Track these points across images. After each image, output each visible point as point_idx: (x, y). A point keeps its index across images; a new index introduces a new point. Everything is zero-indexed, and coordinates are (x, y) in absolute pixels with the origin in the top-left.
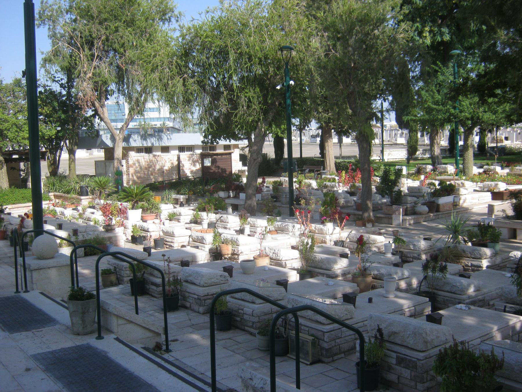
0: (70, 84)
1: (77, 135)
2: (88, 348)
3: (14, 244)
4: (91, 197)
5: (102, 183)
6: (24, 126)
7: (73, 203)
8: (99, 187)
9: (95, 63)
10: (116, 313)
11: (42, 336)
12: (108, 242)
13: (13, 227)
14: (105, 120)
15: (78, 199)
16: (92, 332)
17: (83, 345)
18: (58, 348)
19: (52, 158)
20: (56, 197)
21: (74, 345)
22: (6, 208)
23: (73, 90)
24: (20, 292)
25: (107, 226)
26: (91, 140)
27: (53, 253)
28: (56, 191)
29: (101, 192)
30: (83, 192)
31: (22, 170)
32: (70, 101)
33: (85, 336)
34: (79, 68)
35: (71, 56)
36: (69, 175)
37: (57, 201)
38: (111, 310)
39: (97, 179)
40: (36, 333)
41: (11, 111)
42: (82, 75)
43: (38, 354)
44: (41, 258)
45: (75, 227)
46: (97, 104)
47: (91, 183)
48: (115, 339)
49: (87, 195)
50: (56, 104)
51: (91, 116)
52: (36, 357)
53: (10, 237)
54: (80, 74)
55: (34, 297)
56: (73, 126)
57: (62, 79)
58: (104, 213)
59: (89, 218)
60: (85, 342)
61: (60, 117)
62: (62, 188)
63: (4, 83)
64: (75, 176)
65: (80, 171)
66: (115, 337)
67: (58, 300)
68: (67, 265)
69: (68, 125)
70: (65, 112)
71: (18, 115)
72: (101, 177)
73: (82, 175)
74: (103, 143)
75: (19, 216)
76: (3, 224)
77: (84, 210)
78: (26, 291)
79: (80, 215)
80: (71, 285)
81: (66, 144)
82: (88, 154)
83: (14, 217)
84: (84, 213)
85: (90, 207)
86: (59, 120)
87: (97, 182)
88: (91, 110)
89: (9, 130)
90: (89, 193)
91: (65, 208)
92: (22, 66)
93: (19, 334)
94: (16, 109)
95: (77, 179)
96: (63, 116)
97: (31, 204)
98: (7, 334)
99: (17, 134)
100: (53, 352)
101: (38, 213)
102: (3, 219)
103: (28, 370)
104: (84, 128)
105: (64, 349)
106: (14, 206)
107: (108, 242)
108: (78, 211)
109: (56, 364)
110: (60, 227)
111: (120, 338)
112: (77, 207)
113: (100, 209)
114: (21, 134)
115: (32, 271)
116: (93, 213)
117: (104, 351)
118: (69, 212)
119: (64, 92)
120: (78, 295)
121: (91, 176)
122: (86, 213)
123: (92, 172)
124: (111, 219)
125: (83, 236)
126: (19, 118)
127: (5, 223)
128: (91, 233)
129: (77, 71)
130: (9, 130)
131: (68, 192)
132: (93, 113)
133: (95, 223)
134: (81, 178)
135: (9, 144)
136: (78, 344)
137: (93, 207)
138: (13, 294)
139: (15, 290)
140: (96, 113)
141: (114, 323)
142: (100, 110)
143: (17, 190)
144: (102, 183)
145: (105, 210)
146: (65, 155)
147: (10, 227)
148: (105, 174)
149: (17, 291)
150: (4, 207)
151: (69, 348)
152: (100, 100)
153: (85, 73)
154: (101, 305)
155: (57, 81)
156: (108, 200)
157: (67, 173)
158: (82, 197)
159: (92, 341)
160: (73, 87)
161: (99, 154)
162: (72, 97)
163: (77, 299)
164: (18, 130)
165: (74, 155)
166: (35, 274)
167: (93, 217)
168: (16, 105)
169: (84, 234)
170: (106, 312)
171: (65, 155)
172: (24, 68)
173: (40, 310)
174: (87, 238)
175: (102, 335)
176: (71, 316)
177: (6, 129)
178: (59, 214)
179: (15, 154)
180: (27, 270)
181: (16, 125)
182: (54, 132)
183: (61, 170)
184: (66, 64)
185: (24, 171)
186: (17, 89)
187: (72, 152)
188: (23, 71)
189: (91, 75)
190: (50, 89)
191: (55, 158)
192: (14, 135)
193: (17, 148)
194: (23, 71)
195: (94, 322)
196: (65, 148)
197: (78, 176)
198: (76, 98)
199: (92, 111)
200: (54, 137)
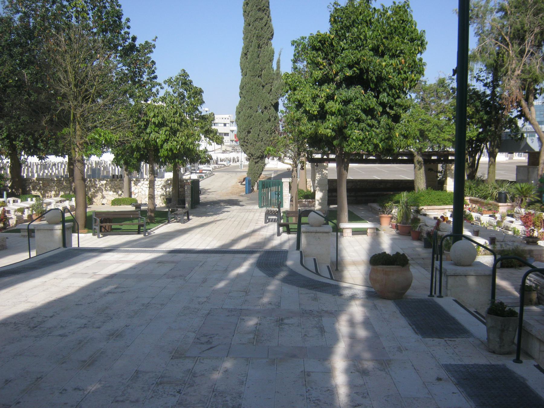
0: (494, 84)
1: (500, 137)
2: (504, 369)
3: (427, 245)
4: (509, 204)
5: (524, 190)
6: (445, 127)
7: (490, 210)
8: (519, 195)
9: (525, 59)
10: (539, 337)
11: (455, 346)
12: (529, 256)
13: (430, 229)
14: (533, 121)
15: (496, 205)
16: (509, 353)
17: (498, 365)
18: (471, 363)
19: (471, 160)
20: (472, 201)
21: (488, 363)
22: (421, 209)
23: (498, 89)
24: (433, 296)
25: (528, 237)
26: (514, 144)
27: (468, 261)
28: (472, 195)
29: (522, 200)
30: (501, 198)
31: (439, 172)
32: (494, 100)
33: (501, 356)
34: (507, 65)
35: (498, 54)
36: (487, 180)
37: (474, 206)
38: (534, 332)
39: (518, 186)
40: (448, 342)
41: (433, 112)
42: (509, 73)
43: (450, 365)
44: (457, 264)
45: (493, 235)
46: (523, 103)
47: (510, 190)
48: (535, 365)
49: (506, 202)
50: (478, 104)
51: (516, 117)
52: (448, 368)
53: (425, 239)
54: (507, 72)
55: (446, 303)
56: (496, 128)
57: (486, 78)
58: (525, 223)
59: (507, 227)
60: (500, 363)
61: (482, 118)
62: (479, 192)
63: (428, 83)
64: (494, 181)
65: (500, 175)
66: (536, 364)
67: (472, 310)
68: (489, 275)
69: (490, 126)
70: (487, 113)
71: (440, 116)
72: (523, 183)
73: (501, 180)
74: (527, 146)
75: (435, 218)
76: (419, 225)
77: (503, 218)
78: (440, 296)
79: (498, 222)
80: (490, 298)
81: (487, 147)
82: (507, 158)
83: (431, 219)
84: (502, 221)
85: (508, 215)
86: (481, 121)
87: (517, 188)
88: (516, 111)
89: (430, 131)
90: (508, 201)
91: (482, 214)
92: (454, 64)
93: (432, 339)
94: (439, 110)
95: (495, 184)
96: (485, 117)
97: (452, 207)
98: (419, 337)
99: (437, 135)
100: (465, 366)
101: (459, 216)
102: (419, 220)
103: (439, 379)
104: (507, 130)
105: (477, 365)
106: (429, 207)
107: (529, 256)
108: (496, 218)
109: (468, 379)
110: (476, 233)
111: (542, 366)
112: (494, 213)
113: (521, 218)
114: (442, 135)
115: (447, 276)
116: (512, 222)
117: (522, 377)
118: (485, 219)
119: (488, 92)
120: (497, 310)
121: (511, 182)
122: (505, 221)
123: (512, 177)
124: (533, 230)
125: (501, 245)
126: (441, 119)
127: (421, 224)
128: (510, 243)
129: (504, 68)
130: (430, 131)
131: (485, 198)
132: (519, 113)
133: (514, 232)
134: (500, 183)
135: (429, 144)
136: (493, 363)
137: (512, 216)
138: (427, 297)
139: (429, 293)
140: (522, 115)
141: (535, 348)
142: (527, 110)
143: (434, 192)
144: (524, 190)
145: (526, 220)
146: (484, 159)
147: (425, 229)
148: (528, 180)
149: (431, 295)
150: (421, 207)
151: (482, 365)
152: (527, 100)
153: (514, 71)
154: (523, 325)
155: (481, 81)
156: (529, 209)
157: (486, 177)
158: (500, 204)
159: (509, 362)
160: (498, 86)
161: (521, 158)
162: (497, 97)
163: (497, 315)
164: (439, 131)
165: (495, 157)
166: (451, 281)
167: (513, 225)
168: (438, 106)
169: (502, 243)
170: (529, 334)
171: (484, 159)
172: (455, 66)
173: (453, 319)
174: (505, 248)
175: (521, 359)
176: (488, 331)
177: (427, 130)
178: (474, 219)
179: (434, 155)
180: (443, 275)
181: (438, 126)
182: (475, 133)
183: (478, 174)
184: (491, 61)
185: (441, 172)
186: (440, 89)
187: (492, 155)
188: (453, 70)
189: (519, 72)
190: (473, 89)
191: (474, 160)
192: (434, 136)
193: (436, 149)
194: (453, 70)
195: (513, 343)
196: (485, 151)
197: (497, 181)
198: (500, 98)
199: (518, 111)
200: (474, 139)
